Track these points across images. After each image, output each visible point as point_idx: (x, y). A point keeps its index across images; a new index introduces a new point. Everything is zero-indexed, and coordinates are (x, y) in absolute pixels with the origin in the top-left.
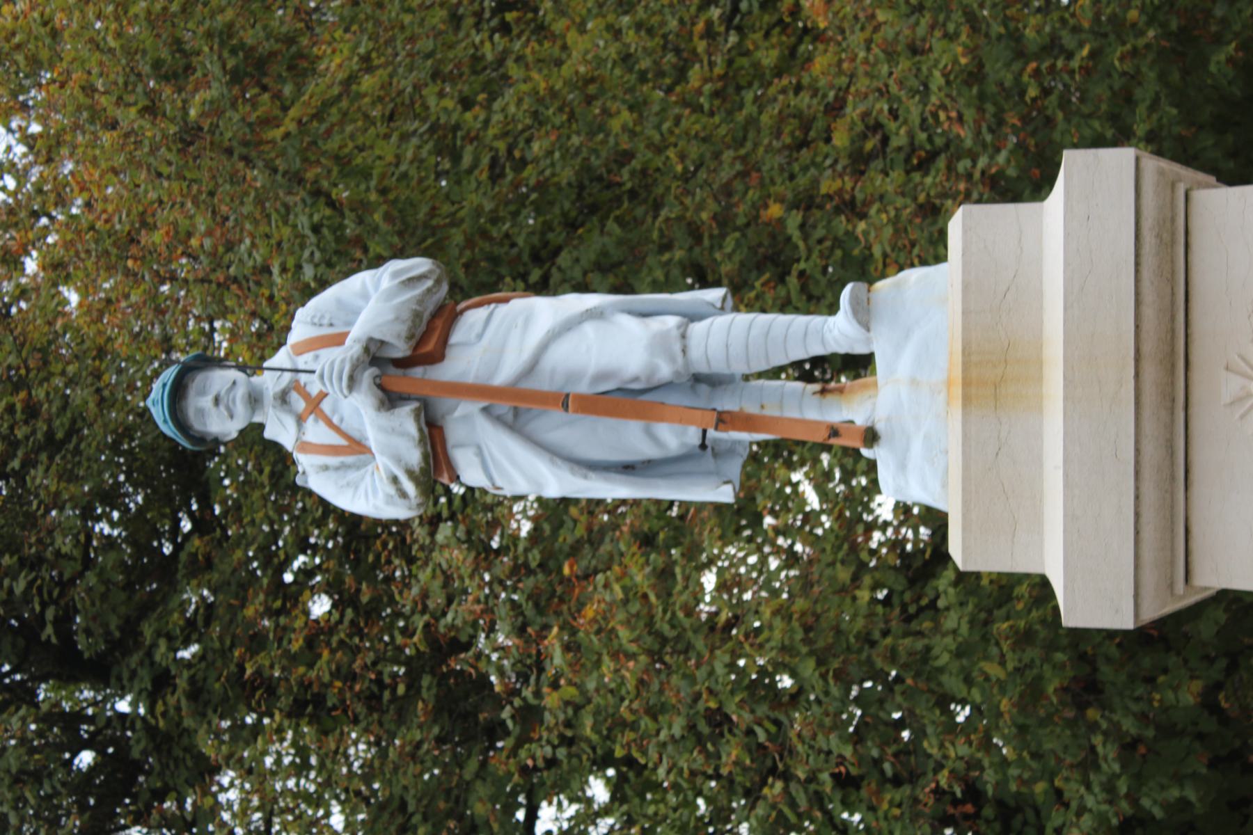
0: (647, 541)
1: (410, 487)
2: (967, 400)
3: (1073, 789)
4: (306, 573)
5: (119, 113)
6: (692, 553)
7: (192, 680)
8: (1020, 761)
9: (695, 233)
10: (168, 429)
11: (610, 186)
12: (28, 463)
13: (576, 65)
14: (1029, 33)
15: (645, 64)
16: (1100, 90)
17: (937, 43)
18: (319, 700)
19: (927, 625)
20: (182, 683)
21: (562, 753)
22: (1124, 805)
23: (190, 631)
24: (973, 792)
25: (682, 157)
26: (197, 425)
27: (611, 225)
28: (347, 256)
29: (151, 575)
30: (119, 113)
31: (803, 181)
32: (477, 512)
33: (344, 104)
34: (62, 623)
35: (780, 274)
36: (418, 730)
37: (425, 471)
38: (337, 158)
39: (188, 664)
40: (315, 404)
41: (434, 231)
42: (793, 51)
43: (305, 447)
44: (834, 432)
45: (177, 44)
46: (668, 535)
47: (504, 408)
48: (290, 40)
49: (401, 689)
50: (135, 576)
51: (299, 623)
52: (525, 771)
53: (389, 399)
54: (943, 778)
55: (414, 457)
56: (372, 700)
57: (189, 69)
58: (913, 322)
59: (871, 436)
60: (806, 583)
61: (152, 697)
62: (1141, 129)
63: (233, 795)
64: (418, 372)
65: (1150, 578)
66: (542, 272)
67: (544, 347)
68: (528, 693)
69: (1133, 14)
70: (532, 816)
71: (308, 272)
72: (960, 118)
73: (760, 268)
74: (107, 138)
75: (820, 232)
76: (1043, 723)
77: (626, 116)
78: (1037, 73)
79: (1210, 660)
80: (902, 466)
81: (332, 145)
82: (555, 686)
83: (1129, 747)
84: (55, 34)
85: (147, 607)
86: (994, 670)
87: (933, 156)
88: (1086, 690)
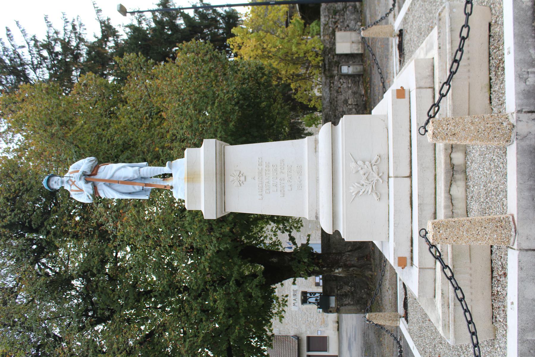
0: (135, 206)
1: (91, 197)
2: (188, 181)
3: (209, 246)
4: (75, 213)
5: (39, 131)
6: (144, 208)
7: (54, 232)
8: (200, 242)
9: (144, 153)
10: (46, 187)
11: (129, 144)
12: (23, 194)
13: (123, 124)
14: (200, 120)
15: (135, 124)
16: (212, 129)
17: (185, 121)
18: (77, 235)
19: (184, 219)
20: (52, 233)
21: (121, 243)
22: (217, 248)
23: (54, 223)
24: (192, 247)
25: (141, 140)
26: (52, 187)
27: (129, 151)
28: (80, 157)
29: (46, 213)
30: (39, 131)
31: (162, 144)
32: (106, 202)
33: (81, 130)
34: (30, 222)
35: (158, 159)
36: (95, 240)
37: (93, 194)
38: (80, 139)
39: (53, 229)
40: (73, 183)
41: (97, 152)
42: (161, 122)
43: (72, 190)
44: (165, 187)
45: (50, 119)
46: (139, 205)
47: (108, 183)
48: (71, 119)
49: (92, 233)
50: (43, 214)
51: (73, 222)
52: (114, 247)
53: (87, 182)
54: (187, 245)
55: (92, 192)
56: (87, 235)
57: (52, 123)
58: (179, 168)
59: (172, 187)
60: (163, 213)
61: (47, 235)
62: (218, 136)
63: (62, 252)
64: (92, 177)
65: (218, 211)
66: (116, 160)
67: (115, 172)
68: (114, 233)
69: (217, 117)
70: (117, 254)
71: (74, 159)
72: (189, 134)
73: (155, 158)
74: (37, 135)
75: (165, 153)
76: (203, 235)
77: (131, 133)
78: (201, 126)
79: (231, 223)
80: (177, 192)
81: (79, 137)
82: (119, 232)
83: (218, 239)
84: (27, 117)
85: (45, 220)
86: (195, 227)
87: (184, 140)
88: (211, 229)
